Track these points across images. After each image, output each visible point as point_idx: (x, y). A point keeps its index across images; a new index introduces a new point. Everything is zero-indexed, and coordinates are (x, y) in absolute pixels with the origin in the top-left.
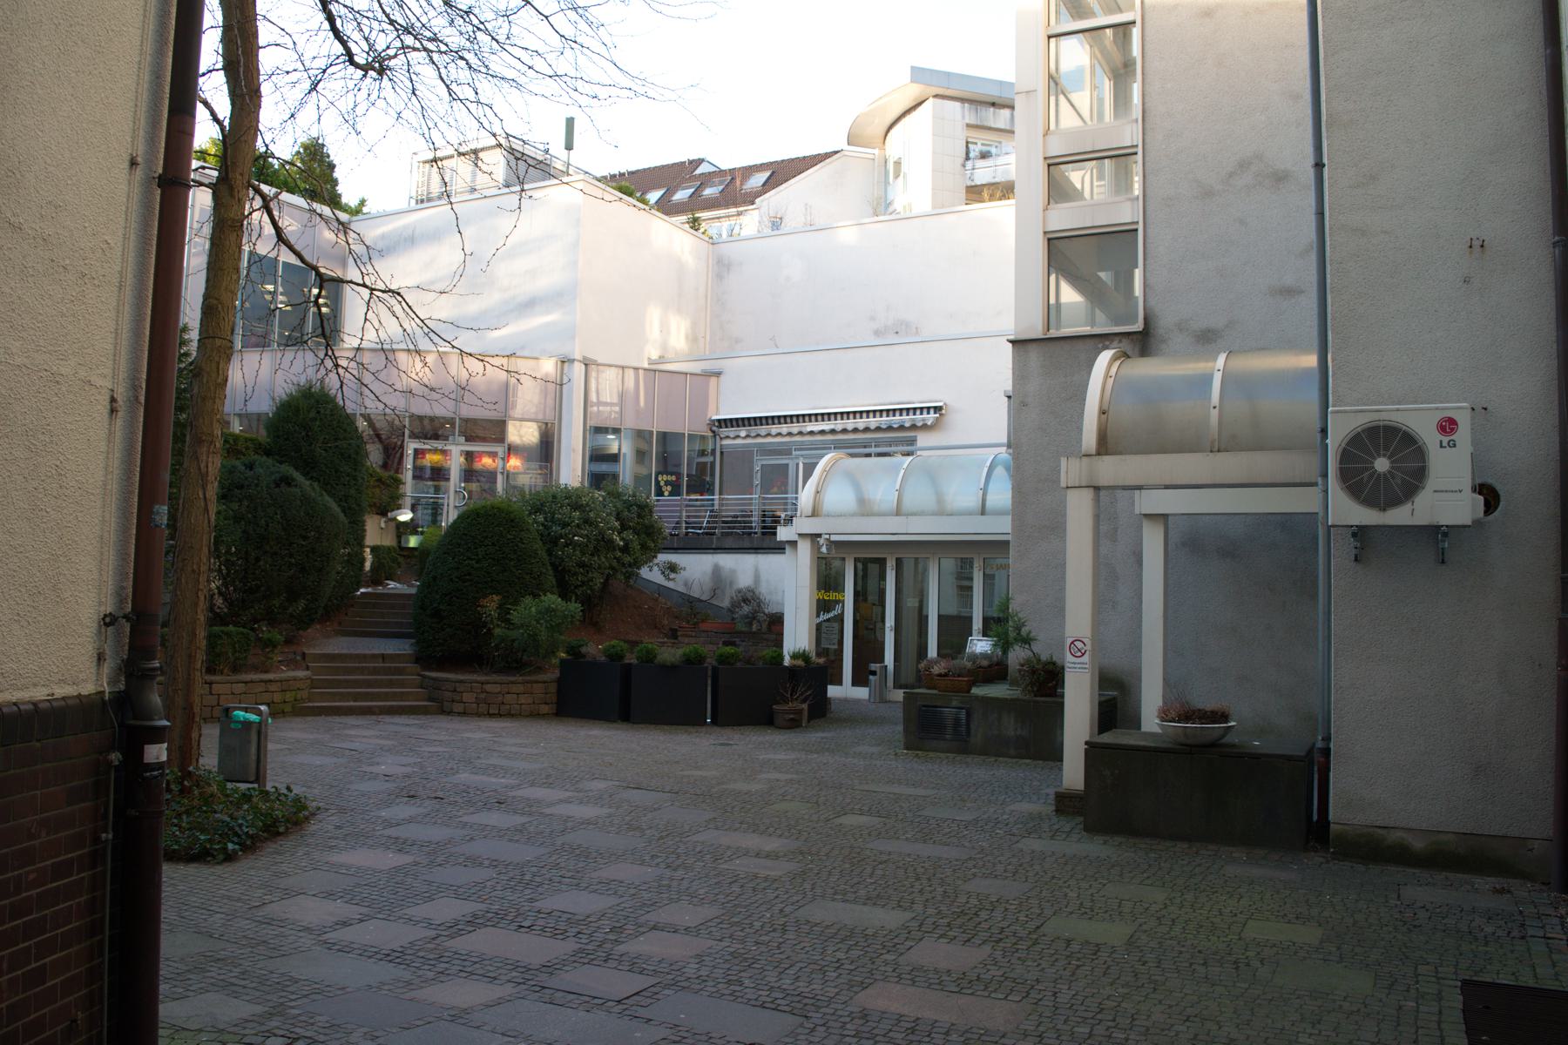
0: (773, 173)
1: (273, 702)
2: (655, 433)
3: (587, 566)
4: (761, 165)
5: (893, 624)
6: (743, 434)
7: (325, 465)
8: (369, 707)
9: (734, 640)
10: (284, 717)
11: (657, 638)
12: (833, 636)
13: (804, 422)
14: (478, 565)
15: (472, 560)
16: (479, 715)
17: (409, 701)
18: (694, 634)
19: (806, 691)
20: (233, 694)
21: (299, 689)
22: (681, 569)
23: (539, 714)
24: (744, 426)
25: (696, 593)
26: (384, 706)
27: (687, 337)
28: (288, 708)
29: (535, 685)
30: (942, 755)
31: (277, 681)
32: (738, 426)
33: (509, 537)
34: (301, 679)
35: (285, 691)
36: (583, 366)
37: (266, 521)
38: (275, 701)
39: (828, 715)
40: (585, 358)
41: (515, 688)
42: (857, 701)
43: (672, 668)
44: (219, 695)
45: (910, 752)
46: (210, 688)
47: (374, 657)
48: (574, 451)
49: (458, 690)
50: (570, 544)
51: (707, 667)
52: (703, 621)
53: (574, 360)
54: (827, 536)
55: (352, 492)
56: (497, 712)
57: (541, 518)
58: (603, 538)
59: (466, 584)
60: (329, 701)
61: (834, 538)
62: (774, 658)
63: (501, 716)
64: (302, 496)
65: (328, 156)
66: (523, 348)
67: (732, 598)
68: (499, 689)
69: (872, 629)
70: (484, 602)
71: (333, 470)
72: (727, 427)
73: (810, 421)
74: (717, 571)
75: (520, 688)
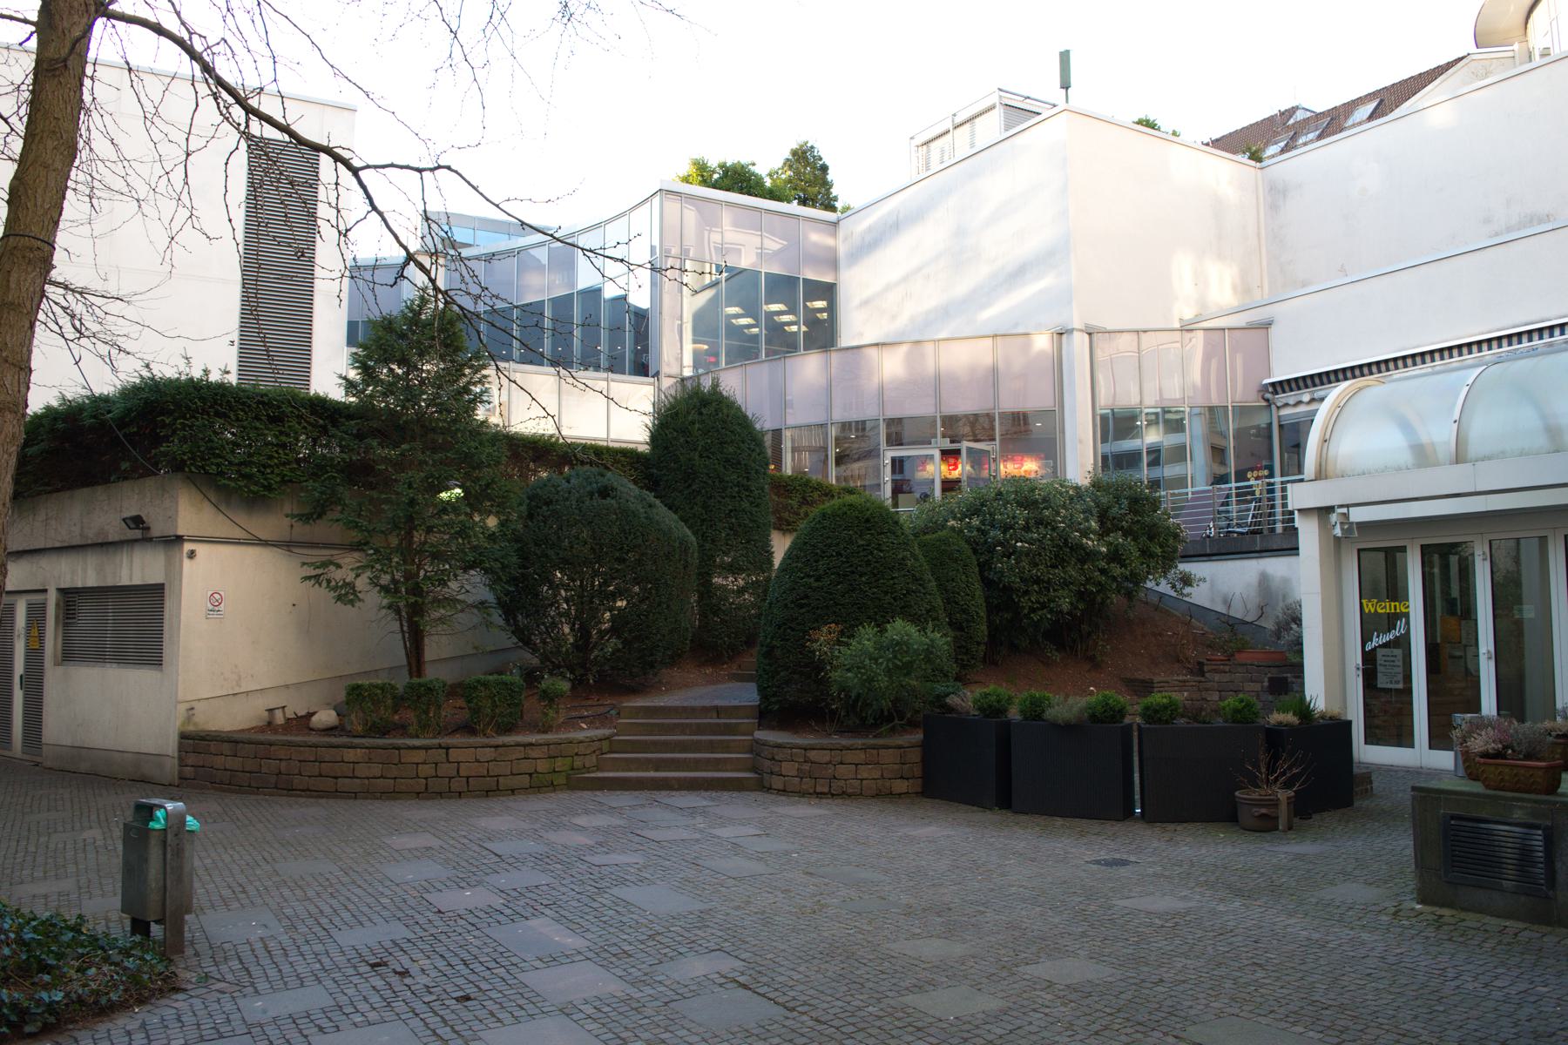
0: (1381, 101)
3: (1043, 581)
4: (1366, 96)
5: (1492, 648)
6: (1306, 398)
7: (707, 474)
8: (665, 779)
9: (1285, 675)
10: (554, 791)
13: (1388, 370)
14: (816, 584)
15: (809, 576)
16: (803, 794)
17: (727, 771)
18: (1227, 668)
19: (1290, 768)
21: (577, 754)
22: (1200, 580)
24: (1307, 387)
25: (1237, 612)
26: (685, 778)
27: (1235, 288)
28: (560, 780)
30: (1493, 922)
31: (541, 745)
32: (1299, 389)
34: (581, 742)
35: (554, 757)
36: (1087, 336)
37: (570, 543)
38: (539, 770)
39: (1357, 804)
41: (850, 757)
42: (1436, 773)
43: (1068, 729)
44: (458, 763)
45: (1428, 909)
46: (447, 754)
47: (705, 710)
48: (1081, 442)
49: (777, 757)
50: (1011, 554)
51: (1130, 726)
52: (1239, 651)
54: (1344, 510)
55: (746, 505)
57: (976, 522)
59: (804, 610)
60: (623, 771)
61: (1358, 515)
63: (833, 795)
64: (619, 508)
65: (821, 159)
66: (1016, 325)
67: (1278, 617)
68: (827, 759)
69: (1460, 657)
70: (814, 634)
71: (717, 480)
72: (1284, 392)
73: (1397, 368)
74: (1264, 580)
75: (860, 757)
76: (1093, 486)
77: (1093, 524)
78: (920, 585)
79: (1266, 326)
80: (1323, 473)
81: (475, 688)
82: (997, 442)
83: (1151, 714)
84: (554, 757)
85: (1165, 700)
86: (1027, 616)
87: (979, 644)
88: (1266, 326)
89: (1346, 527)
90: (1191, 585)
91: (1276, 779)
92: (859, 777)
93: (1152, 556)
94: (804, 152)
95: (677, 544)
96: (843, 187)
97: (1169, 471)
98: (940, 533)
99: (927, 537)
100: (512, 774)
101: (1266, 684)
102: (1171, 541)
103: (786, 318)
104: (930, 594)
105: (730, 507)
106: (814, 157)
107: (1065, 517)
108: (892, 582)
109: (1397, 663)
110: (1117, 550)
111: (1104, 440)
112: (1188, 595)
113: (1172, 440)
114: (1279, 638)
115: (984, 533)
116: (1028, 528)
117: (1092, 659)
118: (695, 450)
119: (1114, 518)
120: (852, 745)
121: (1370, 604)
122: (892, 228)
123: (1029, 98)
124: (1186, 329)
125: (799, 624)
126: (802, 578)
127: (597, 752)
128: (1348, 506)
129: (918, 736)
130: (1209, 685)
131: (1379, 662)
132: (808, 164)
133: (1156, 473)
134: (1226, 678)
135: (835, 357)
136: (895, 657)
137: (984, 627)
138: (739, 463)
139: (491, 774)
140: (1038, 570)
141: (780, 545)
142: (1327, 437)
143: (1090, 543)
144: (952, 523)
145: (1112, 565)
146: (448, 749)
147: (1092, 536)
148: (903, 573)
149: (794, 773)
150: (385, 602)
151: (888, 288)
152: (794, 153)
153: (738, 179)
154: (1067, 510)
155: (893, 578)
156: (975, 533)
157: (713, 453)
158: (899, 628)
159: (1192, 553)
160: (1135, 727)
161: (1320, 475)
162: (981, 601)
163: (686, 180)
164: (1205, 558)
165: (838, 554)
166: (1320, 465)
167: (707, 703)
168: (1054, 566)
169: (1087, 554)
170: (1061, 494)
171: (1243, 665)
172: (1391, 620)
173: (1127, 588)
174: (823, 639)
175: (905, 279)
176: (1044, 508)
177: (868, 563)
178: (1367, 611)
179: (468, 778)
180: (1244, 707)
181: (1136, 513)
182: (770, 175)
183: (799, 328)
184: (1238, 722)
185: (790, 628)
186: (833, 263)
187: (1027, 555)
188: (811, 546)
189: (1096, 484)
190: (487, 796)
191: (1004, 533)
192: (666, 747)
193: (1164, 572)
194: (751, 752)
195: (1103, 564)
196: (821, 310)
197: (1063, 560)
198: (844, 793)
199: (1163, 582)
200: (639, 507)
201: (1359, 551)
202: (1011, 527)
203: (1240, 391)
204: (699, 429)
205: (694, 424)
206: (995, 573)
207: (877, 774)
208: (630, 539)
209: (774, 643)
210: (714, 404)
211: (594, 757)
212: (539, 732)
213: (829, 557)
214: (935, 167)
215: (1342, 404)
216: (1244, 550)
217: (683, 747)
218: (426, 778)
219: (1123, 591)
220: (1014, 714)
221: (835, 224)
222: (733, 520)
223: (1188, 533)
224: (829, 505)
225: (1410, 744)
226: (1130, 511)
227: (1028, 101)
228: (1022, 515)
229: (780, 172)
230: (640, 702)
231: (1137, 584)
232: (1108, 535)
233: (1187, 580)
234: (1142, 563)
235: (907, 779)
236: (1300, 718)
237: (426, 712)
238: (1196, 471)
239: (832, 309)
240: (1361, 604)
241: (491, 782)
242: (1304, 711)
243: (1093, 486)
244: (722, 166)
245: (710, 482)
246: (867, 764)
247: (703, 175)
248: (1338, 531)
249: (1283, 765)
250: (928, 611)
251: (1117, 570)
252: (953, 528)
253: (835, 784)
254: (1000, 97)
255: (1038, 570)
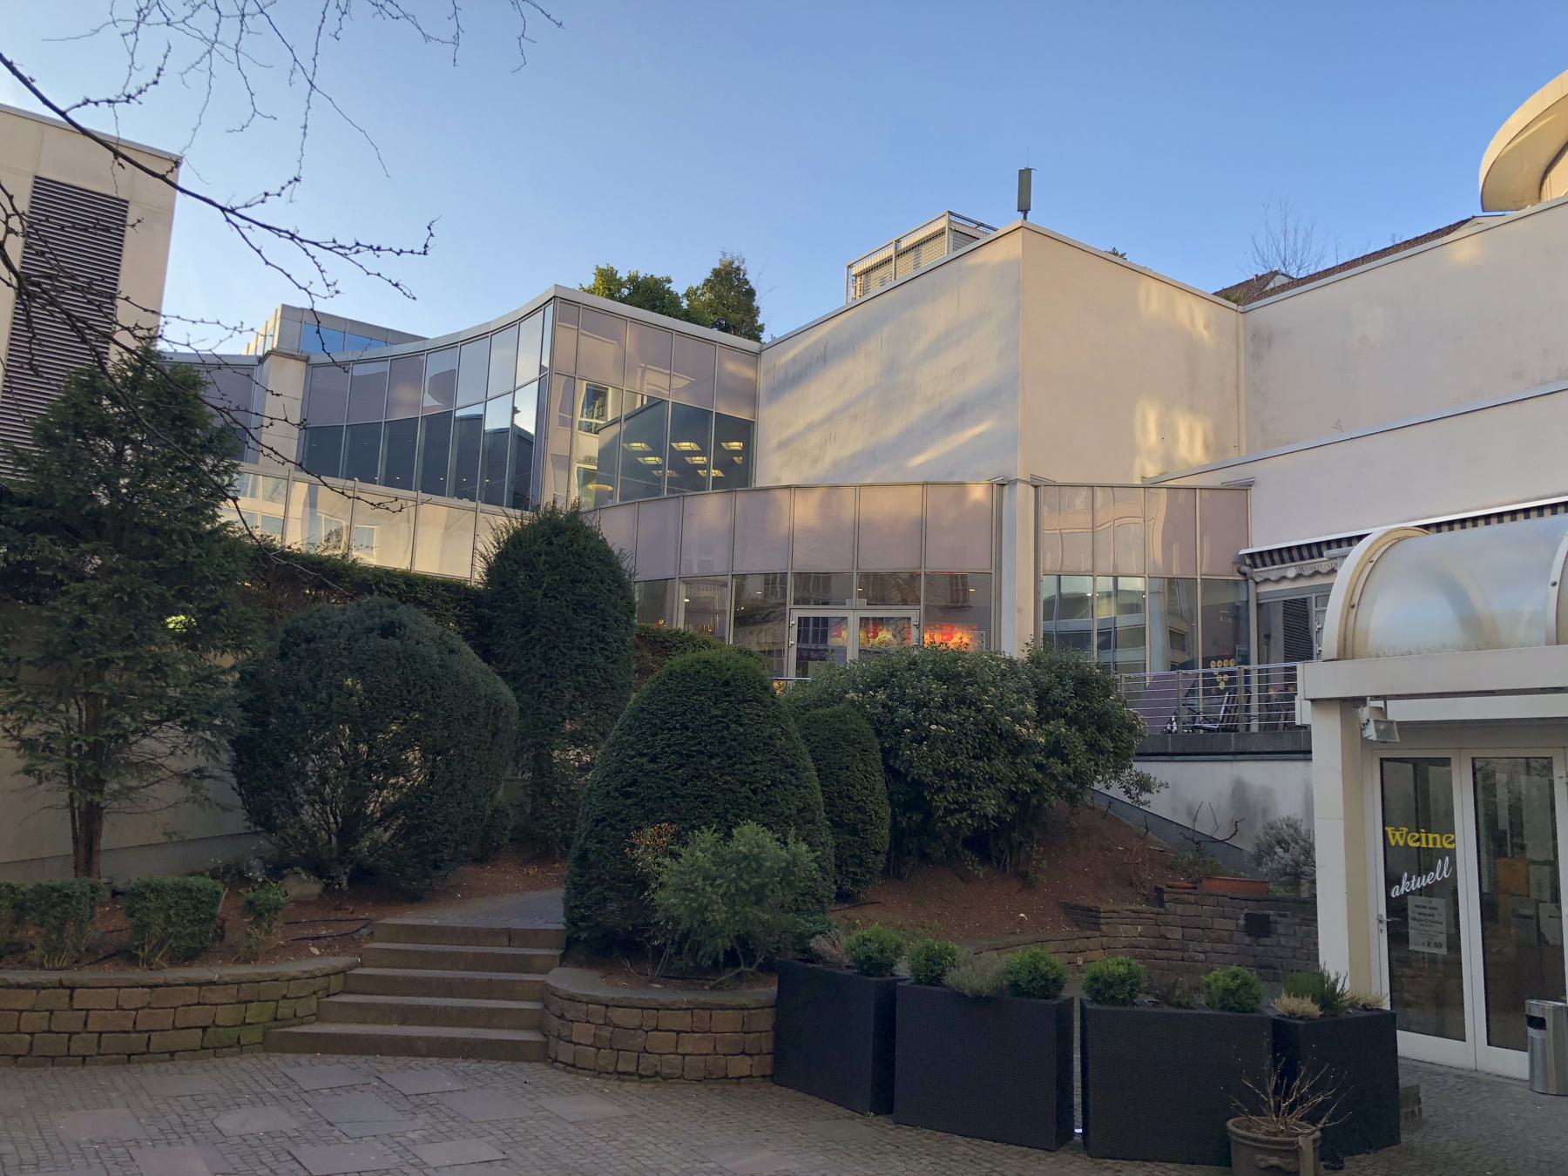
3: (963, 775)
4: (1344, 264)
6: (1291, 573)
7: (552, 619)
9: (1267, 912)
11: (1131, 903)
12: (1437, 927)
15: (642, 755)
18: (1192, 898)
20: (118, 1008)
21: (284, 997)
23: (726, 1077)
24: (1292, 560)
25: (1204, 826)
28: (254, 1035)
29: (717, 1014)
32: (1283, 562)
33: (715, 712)
34: (294, 979)
35: (246, 1002)
36: (1032, 490)
40: (1033, 477)
41: (670, 1020)
42: (1498, 1084)
43: (979, 1001)
44: (88, 1010)
46: (71, 997)
47: (493, 935)
48: (1019, 611)
49: (567, 1016)
50: (925, 739)
53: (1016, 481)
54: (1380, 704)
55: (599, 659)
56: (687, 1058)
57: (881, 696)
58: (994, 726)
61: (1399, 712)
62: (1233, 993)
63: (641, 1076)
64: (405, 651)
67: (1258, 838)
68: (637, 1022)
72: (1264, 565)
74: (1239, 789)
75: (685, 1020)
76: (1032, 662)
77: (1029, 707)
78: (792, 774)
79: (1246, 487)
80: (1349, 651)
81: (142, 896)
82: (922, 607)
83: (1101, 988)
84: (246, 1002)
85: (1122, 969)
86: (942, 819)
87: (877, 853)
88: (1246, 487)
89: (1382, 727)
90: (1149, 791)
91: (1292, 1107)
92: (680, 1050)
93: (1101, 752)
94: (728, 273)
95: (482, 703)
96: (775, 317)
97: (1124, 655)
98: (836, 707)
99: (820, 711)
100: (175, 1028)
101: (1242, 922)
102: (1126, 734)
103: (698, 460)
104: (805, 787)
105: (578, 662)
106: (739, 280)
107: (994, 696)
108: (752, 768)
109: (1437, 918)
110: (1058, 742)
111: (1048, 617)
112: (1146, 803)
113: (1124, 621)
114: (1259, 865)
115: (891, 710)
116: (947, 706)
117: (1025, 875)
118: (539, 587)
119: (1056, 702)
120: (673, 1003)
121: (1397, 834)
122: (821, 360)
123: (982, 225)
124: (1149, 486)
125: (622, 821)
126: (632, 757)
127: (319, 994)
128: (1385, 698)
129: (767, 991)
130: (1169, 918)
131: (1410, 914)
132: (732, 287)
133: (1107, 657)
134: (1191, 910)
135: (742, 498)
136: (740, 877)
137: (885, 832)
138: (594, 606)
139: (139, 1027)
140: (957, 761)
142: (1355, 600)
143: (1023, 730)
144: (851, 695)
145: (1051, 760)
146: (73, 988)
147: (1027, 722)
148: (769, 756)
150: (21, 763)
151: (811, 427)
152: (716, 273)
153: (650, 294)
154: (996, 687)
155: (754, 763)
156: (880, 709)
157: (563, 594)
158: (750, 835)
159: (1150, 751)
160: (1077, 1006)
161: (1346, 652)
162: (883, 798)
163: (591, 291)
164: (1166, 758)
165: (685, 727)
166: (1345, 636)
167: (498, 924)
168: (976, 758)
169: (1022, 745)
170: (990, 668)
171: (1213, 895)
172: (1423, 861)
173: (1069, 790)
174: (646, 846)
175: (829, 418)
176: (968, 684)
177: (722, 741)
178: (1393, 843)
179: (100, 1033)
180: (1239, 987)
181: (1084, 697)
182: (687, 295)
183: (709, 472)
184: (1231, 1009)
185: (610, 825)
186: (753, 399)
187: (943, 741)
188: (648, 713)
189: (1035, 660)
190: (129, 1062)
191: (916, 712)
192: (425, 987)
193: (1116, 773)
194: (542, 1000)
195: (1040, 758)
196: (736, 453)
197: (991, 751)
198: (657, 1074)
199: (1115, 784)
200: (434, 651)
201: (1382, 760)
202: (925, 705)
203: (1209, 562)
204: (545, 562)
205: (540, 555)
206: (902, 762)
207: (708, 1048)
208: (413, 693)
209: (588, 845)
210: (568, 533)
211: (313, 1002)
212: (238, 961)
213: (670, 730)
214: (874, 292)
215: (1375, 558)
216: (1215, 750)
217: (448, 988)
218: (32, 1034)
219: (1064, 794)
220: (903, 969)
221: (757, 355)
222: (581, 678)
223: (1145, 725)
224: (677, 661)
225: (1456, 1032)
226: (1076, 694)
227: (981, 228)
228: (938, 690)
229: (699, 292)
230: (411, 917)
231: (1082, 785)
232: (1048, 722)
233: (1144, 785)
234: (1089, 760)
235: (751, 1055)
236: (1322, 1008)
237: (60, 930)
238: (1153, 657)
239: (748, 452)
240: (1384, 830)
241: (137, 1041)
242: (1327, 996)
243: (1032, 662)
244: (633, 280)
245: (553, 628)
247: (608, 282)
248: (1371, 733)
249: (1301, 1085)
250: (800, 811)
251: (1057, 767)
252: (852, 702)
254: (950, 221)
255: (957, 761)
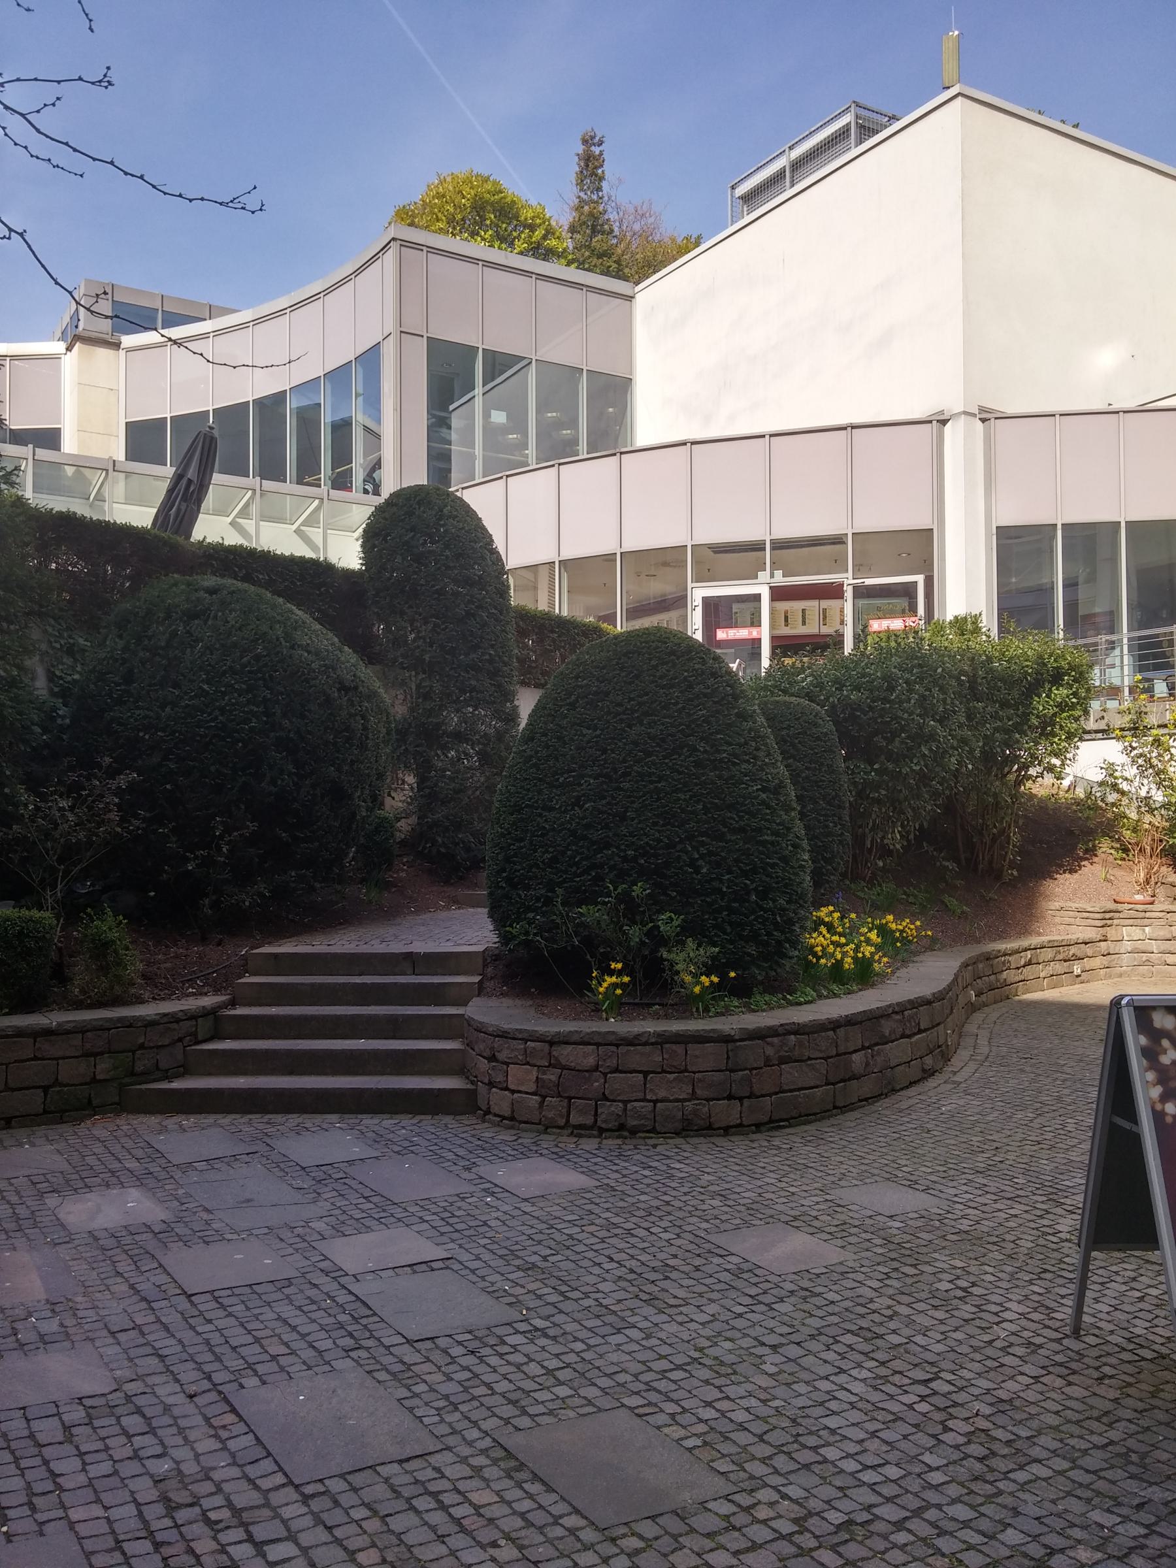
1: (57, 1083)
2: (1123, 525)
31: (68, 1032)
35: (95, 1055)
49: (500, 1056)
68: (591, 1061)
141: (526, 703)
149: (532, 1087)
207: (684, 1091)
246: (664, 1071)
253: (608, 1110)
